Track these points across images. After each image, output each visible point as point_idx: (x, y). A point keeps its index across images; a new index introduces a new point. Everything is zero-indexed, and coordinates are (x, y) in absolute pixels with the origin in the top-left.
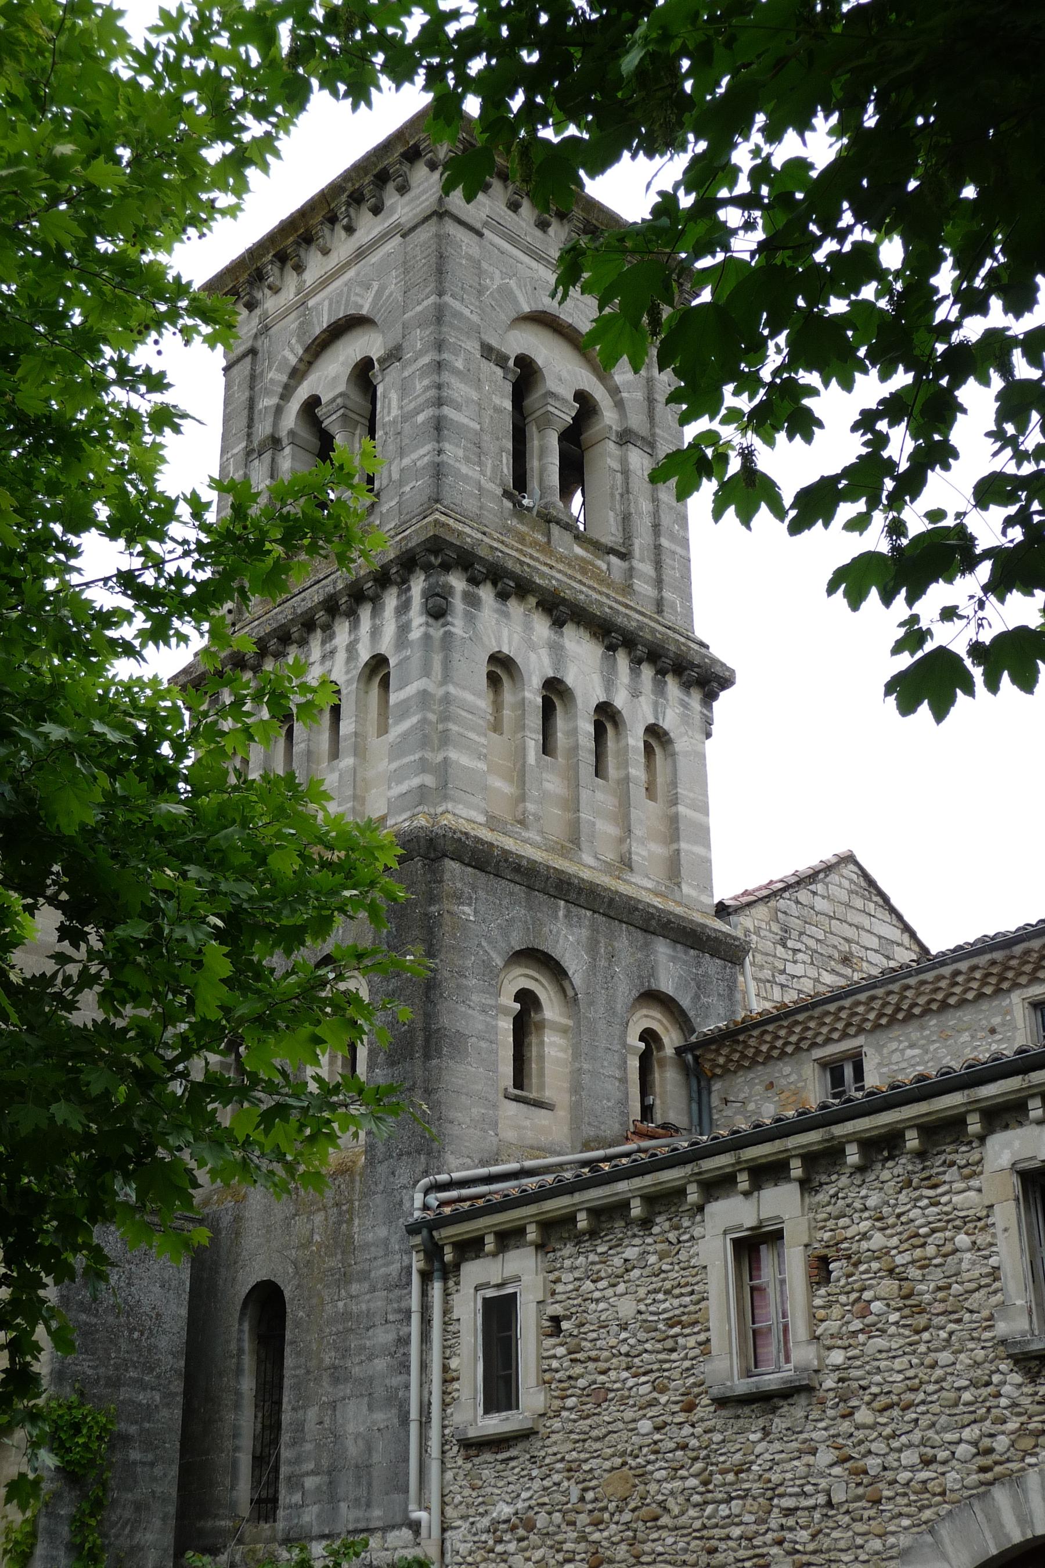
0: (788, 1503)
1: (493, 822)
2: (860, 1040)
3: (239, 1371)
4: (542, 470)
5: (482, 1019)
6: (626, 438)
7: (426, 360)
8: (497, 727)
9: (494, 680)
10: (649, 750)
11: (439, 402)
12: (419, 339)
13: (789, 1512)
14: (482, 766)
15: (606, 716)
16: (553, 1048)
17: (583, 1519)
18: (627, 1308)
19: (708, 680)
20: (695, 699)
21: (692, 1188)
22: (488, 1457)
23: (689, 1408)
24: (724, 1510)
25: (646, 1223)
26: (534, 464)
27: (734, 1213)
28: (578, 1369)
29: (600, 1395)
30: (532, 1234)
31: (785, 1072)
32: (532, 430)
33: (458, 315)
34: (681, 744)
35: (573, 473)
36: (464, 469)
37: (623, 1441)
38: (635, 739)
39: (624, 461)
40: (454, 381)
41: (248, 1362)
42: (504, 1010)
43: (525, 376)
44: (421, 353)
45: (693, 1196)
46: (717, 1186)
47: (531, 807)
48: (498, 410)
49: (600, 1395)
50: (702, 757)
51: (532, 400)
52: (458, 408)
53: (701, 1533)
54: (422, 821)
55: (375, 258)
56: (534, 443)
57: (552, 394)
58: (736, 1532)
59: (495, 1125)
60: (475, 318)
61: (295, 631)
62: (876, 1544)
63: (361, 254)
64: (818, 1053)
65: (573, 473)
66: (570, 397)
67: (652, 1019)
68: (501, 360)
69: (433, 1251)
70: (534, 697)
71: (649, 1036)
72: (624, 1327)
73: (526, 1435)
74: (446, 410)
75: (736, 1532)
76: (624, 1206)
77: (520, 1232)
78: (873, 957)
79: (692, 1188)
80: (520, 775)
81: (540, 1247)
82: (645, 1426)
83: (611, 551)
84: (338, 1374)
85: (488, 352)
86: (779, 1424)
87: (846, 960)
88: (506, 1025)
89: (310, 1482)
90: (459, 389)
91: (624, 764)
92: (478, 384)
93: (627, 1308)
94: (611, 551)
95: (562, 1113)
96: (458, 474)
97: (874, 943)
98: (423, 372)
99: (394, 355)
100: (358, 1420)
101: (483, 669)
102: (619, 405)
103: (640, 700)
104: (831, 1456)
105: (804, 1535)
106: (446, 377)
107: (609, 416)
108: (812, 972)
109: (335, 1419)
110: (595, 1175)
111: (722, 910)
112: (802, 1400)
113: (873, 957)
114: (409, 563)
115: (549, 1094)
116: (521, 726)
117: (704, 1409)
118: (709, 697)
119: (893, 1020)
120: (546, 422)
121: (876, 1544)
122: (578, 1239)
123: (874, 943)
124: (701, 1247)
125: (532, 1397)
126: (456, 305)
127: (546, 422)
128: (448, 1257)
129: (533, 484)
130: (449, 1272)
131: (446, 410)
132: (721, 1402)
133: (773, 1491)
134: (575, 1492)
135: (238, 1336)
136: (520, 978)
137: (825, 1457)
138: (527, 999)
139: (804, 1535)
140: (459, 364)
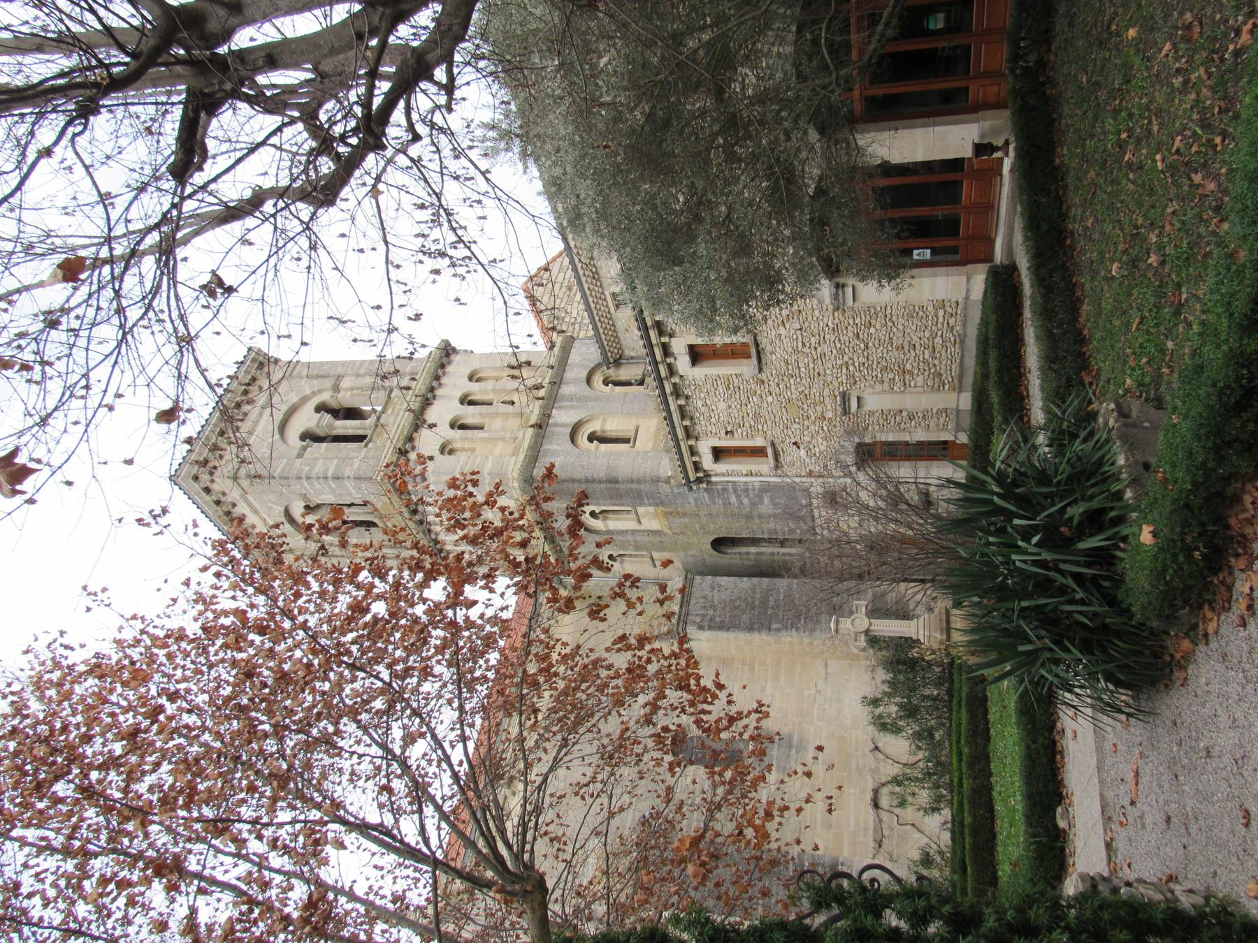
0: (800, 345)
1: (515, 453)
2: (607, 293)
3: (748, 553)
4: (353, 428)
5: (601, 459)
6: (336, 388)
7: (306, 484)
8: (473, 450)
9: (451, 452)
10: (478, 380)
11: (326, 478)
12: (296, 486)
13: (804, 344)
14: (490, 458)
15: (466, 400)
16: (613, 426)
17: (806, 423)
18: (722, 405)
19: (447, 351)
20: (456, 358)
21: (673, 380)
22: (781, 459)
23: (763, 382)
24: (803, 370)
25: (687, 398)
26: (351, 432)
27: (682, 363)
28: (747, 424)
29: (757, 416)
30: (692, 442)
31: (620, 325)
32: (335, 433)
33: (283, 470)
34: (476, 365)
35: (352, 413)
36: (356, 466)
37: (776, 408)
38: (474, 387)
39: (347, 390)
40: (316, 470)
41: (744, 550)
42: (597, 448)
43: (311, 437)
44: (303, 486)
45: (676, 380)
46: (672, 370)
47: (508, 435)
48: (327, 450)
49: (757, 416)
50: (482, 354)
51: (321, 433)
52: (327, 469)
53: (812, 378)
54: (516, 485)
55: (257, 506)
56: (341, 432)
57: (318, 425)
58: (811, 365)
59: (646, 453)
60: (284, 461)
61: (445, 360)
62: (816, 312)
63: (255, 511)
64: (612, 310)
65: (352, 413)
66: (318, 415)
67: (598, 379)
68: (304, 449)
69: (699, 480)
70: (460, 433)
71: (606, 383)
72: (730, 407)
73: (773, 444)
74: (329, 474)
75: (811, 365)
76: (680, 407)
77: (691, 447)
78: (568, 276)
79: (673, 380)
80: (493, 440)
81: (697, 439)
82: (770, 399)
83: (389, 397)
84: (748, 517)
85: (300, 456)
86: (769, 348)
87: (570, 289)
88: (603, 447)
89: (792, 526)
90: (319, 469)
91: (486, 392)
92: (317, 459)
93: (722, 405)
94: (389, 397)
95: (640, 422)
96: (359, 469)
97: (561, 275)
98: (312, 485)
99: (304, 497)
100: (766, 506)
101: (447, 457)
102: (320, 392)
103: (455, 383)
104: (782, 328)
105: (813, 339)
106: (314, 475)
107: (326, 397)
108: (576, 304)
109: (766, 518)
110: (669, 418)
111: (552, 347)
112: (759, 338)
113: (568, 276)
114: (402, 490)
115: (632, 428)
116: (472, 440)
117: (763, 376)
118: (454, 350)
119: (598, 280)
120: (330, 426)
121: (816, 312)
122: (694, 424)
123: (561, 275)
124: (697, 377)
125: (759, 442)
126: (279, 470)
127: (330, 426)
128: (701, 475)
129: (360, 432)
130: (707, 475)
131: (329, 474)
132: (760, 370)
133: (796, 350)
134: (796, 426)
135: (734, 556)
136: (582, 439)
137: (782, 331)
138: (592, 438)
139: (813, 339)
140: (307, 468)
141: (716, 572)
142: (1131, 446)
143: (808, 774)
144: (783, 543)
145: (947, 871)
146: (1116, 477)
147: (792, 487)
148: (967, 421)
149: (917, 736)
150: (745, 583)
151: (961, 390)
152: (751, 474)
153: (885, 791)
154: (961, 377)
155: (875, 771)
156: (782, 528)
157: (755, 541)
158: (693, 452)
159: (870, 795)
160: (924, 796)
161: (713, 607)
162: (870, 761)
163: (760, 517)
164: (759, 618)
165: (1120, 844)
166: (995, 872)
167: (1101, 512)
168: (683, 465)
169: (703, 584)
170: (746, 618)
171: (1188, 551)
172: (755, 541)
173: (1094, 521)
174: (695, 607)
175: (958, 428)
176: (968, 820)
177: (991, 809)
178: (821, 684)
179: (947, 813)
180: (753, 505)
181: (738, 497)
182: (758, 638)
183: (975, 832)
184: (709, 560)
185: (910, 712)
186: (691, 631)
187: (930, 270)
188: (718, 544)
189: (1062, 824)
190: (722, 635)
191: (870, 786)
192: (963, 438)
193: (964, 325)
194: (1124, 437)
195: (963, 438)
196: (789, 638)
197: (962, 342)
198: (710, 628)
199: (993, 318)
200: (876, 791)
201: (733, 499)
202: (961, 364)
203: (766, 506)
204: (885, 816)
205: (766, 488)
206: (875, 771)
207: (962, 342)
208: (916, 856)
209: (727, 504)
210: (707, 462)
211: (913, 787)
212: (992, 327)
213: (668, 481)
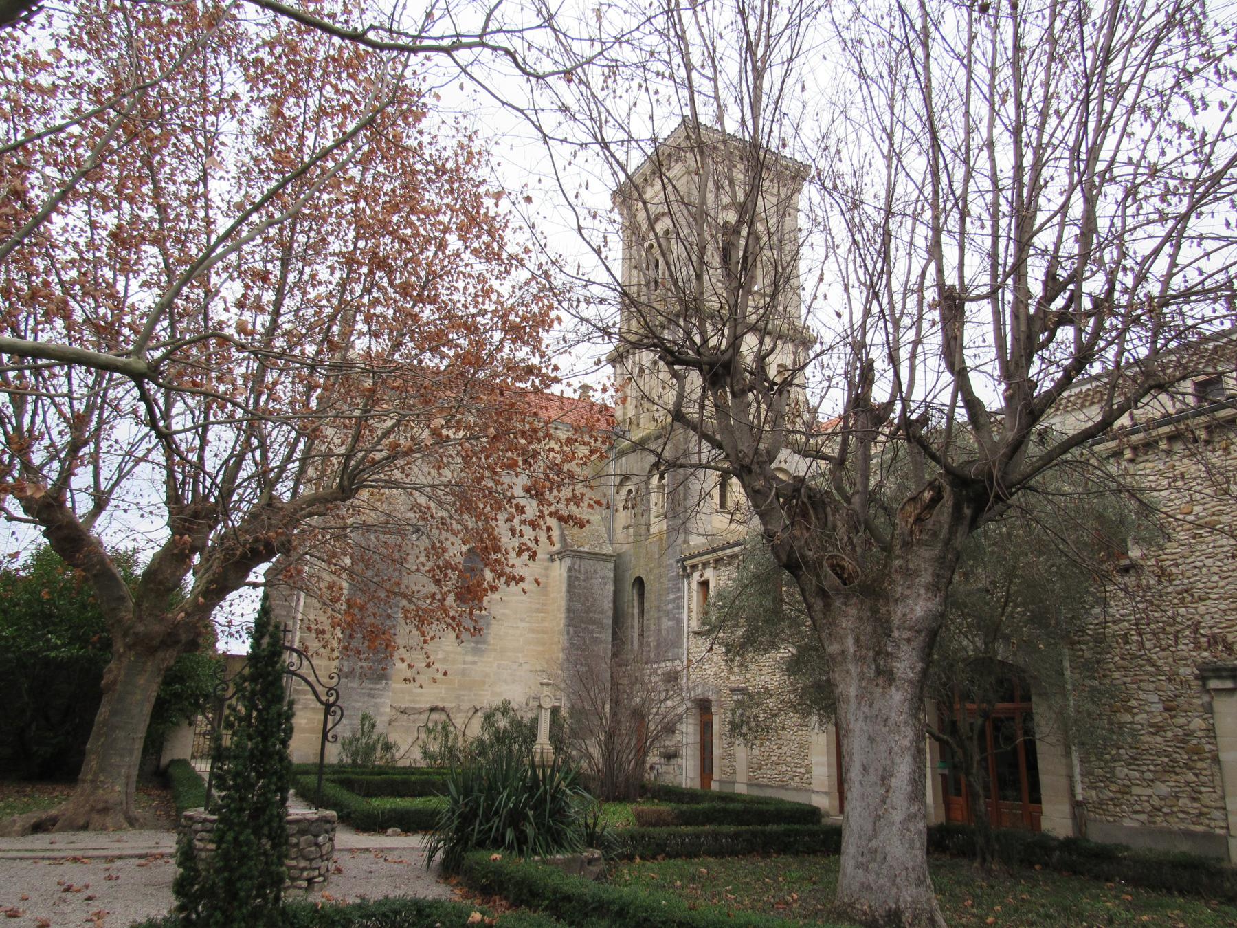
41: (636, 603)
69: (684, 569)
84: (659, 609)
130: (689, 576)
135: (630, 594)
141: (618, 580)
142: (568, 864)
143: (428, 666)
144: (641, 635)
145: (382, 763)
146: (548, 852)
147: (677, 644)
148: (727, 789)
149: (481, 742)
150: (608, 605)
151: (749, 785)
152: (690, 611)
153: (443, 717)
154: (760, 786)
155: (459, 709)
156: (652, 640)
157: (642, 612)
158: (705, 565)
159: (441, 705)
160: (434, 747)
161: (587, 579)
162: (466, 705)
163: (659, 618)
164: (578, 615)
165: (367, 854)
166: (376, 796)
167: (526, 841)
168: (694, 557)
169: (608, 570)
170: (578, 606)
171: (485, 876)
172: (642, 612)
173: (522, 839)
174: (587, 564)
175: (721, 782)
176: (413, 778)
177: (420, 795)
178: (526, 667)
179: (423, 764)
180: (668, 613)
181: (673, 601)
182: (562, 615)
183: (404, 782)
184: (628, 574)
185: (499, 737)
186: (568, 561)
187: (834, 760)
188: (639, 582)
189: (390, 831)
190: (564, 587)
191: (447, 705)
192: (715, 786)
193: (795, 789)
194: (574, 860)
195: (715, 786)
196: (562, 640)
197: (782, 787)
198: (569, 577)
199: (772, 808)
200: (443, 710)
201: (672, 596)
202: (767, 786)
203: (667, 623)
204: (424, 716)
205: (679, 623)
206: (459, 709)
207: (782, 787)
208: (391, 739)
209: (668, 591)
210: (696, 577)
211: (441, 739)
212: (764, 807)
213: (686, 542)
